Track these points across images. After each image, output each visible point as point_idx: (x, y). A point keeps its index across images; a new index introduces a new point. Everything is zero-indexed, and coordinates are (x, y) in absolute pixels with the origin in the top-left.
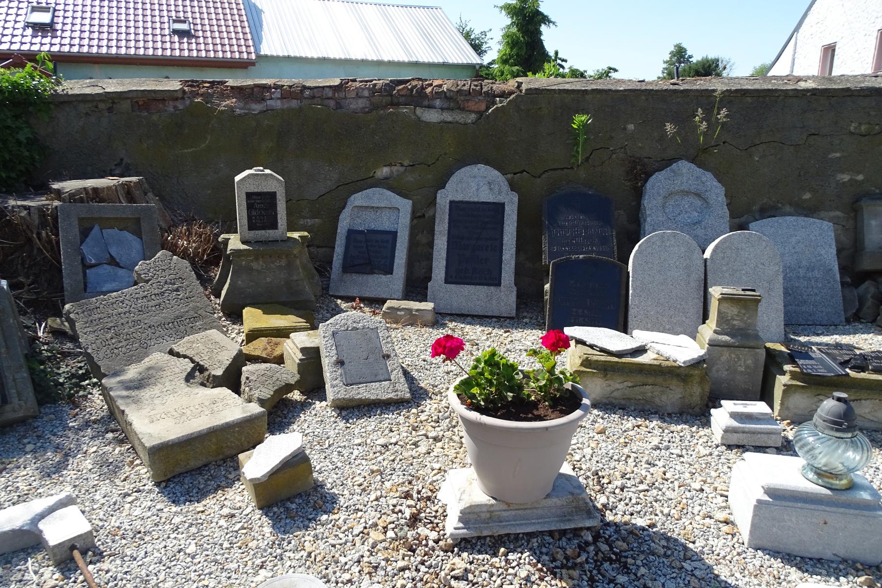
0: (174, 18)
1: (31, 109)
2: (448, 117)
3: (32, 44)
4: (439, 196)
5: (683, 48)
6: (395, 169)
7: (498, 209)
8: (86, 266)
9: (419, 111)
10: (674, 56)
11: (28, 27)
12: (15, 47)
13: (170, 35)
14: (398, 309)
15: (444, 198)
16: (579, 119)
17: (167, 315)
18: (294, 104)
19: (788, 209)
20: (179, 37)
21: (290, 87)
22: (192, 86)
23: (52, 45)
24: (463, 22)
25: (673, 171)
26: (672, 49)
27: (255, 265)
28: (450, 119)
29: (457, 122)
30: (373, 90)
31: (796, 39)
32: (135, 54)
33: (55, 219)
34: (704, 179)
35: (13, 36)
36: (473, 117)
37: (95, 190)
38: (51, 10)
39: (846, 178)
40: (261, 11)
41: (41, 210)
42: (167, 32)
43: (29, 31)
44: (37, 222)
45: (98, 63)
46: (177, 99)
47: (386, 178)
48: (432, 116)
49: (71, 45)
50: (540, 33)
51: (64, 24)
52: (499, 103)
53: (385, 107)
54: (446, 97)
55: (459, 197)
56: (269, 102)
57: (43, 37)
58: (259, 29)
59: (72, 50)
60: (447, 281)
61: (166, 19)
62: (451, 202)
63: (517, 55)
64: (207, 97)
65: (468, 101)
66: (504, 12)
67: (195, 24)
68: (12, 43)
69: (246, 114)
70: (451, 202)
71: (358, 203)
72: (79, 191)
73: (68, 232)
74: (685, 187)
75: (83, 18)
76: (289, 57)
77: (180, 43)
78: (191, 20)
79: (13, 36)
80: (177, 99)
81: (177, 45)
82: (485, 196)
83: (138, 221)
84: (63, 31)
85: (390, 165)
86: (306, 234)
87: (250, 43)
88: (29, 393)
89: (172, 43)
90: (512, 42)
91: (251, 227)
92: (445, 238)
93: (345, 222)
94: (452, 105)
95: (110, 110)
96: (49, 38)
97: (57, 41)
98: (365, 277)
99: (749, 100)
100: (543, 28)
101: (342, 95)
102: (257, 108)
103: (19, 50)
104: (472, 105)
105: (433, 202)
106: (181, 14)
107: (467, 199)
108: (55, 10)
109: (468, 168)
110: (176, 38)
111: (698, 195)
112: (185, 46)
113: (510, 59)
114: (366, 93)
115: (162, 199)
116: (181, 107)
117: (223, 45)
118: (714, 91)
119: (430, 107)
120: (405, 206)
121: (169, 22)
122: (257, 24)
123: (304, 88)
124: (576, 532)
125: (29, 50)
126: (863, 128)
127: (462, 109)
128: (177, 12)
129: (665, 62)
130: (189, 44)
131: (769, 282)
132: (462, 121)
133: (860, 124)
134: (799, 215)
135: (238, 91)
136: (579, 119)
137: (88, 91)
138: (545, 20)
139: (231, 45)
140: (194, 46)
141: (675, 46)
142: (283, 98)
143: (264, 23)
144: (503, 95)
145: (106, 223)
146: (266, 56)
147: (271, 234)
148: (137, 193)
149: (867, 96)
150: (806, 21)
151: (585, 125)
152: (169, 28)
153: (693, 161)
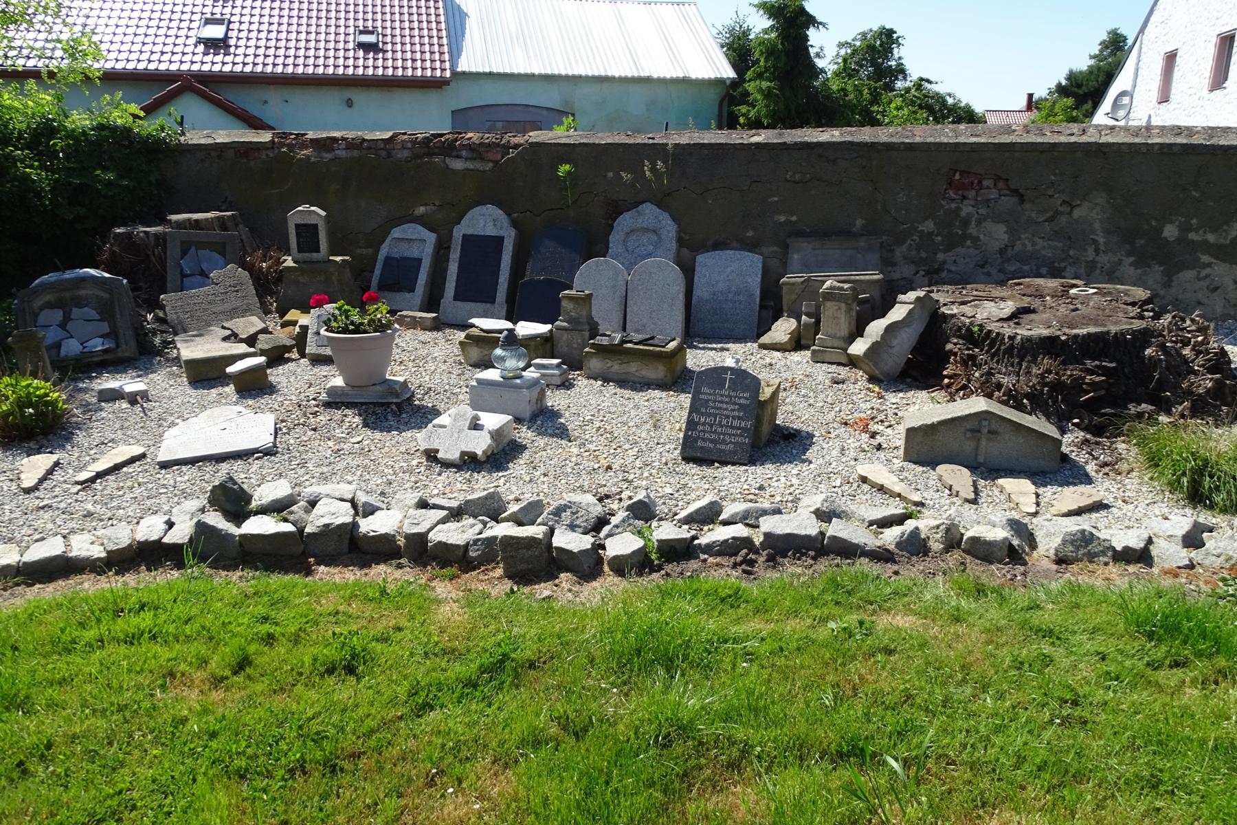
0: (361, 28)
1: (160, 156)
2: (470, 165)
3: (203, 63)
4: (455, 230)
5: (1121, 36)
6: (428, 207)
7: (500, 240)
8: (183, 276)
9: (448, 160)
10: (1107, 47)
11: (200, 43)
12: (185, 67)
13: (354, 49)
14: (406, 316)
15: (459, 232)
16: (565, 168)
17: (228, 306)
18: (355, 153)
19: (735, 244)
20: (364, 51)
21: (353, 139)
22: (281, 138)
23: (224, 63)
24: (741, 17)
25: (638, 212)
26: (1105, 37)
27: (301, 279)
28: (472, 167)
29: (478, 170)
30: (414, 142)
31: (1141, 43)
32: (313, 74)
33: (165, 241)
34: (661, 218)
35: (184, 54)
36: (490, 165)
37: (197, 221)
38: (226, 22)
39: (782, 218)
40: (466, 14)
41: (156, 235)
42: (351, 45)
43: (201, 48)
44: (153, 243)
45: (273, 84)
46: (268, 149)
47: (422, 216)
48: (457, 165)
49: (245, 64)
50: (806, 38)
51: (238, 39)
52: (512, 153)
53: (421, 157)
54: (471, 148)
55: (470, 232)
56: (337, 152)
57: (215, 54)
58: (460, 39)
59: (245, 70)
60: (456, 299)
61: (351, 30)
62: (464, 236)
63: (776, 68)
64: (291, 146)
65: (487, 152)
66: (761, 12)
67: (384, 36)
68: (182, 62)
69: (318, 162)
70: (464, 236)
71: (396, 235)
72: (185, 221)
73: (173, 250)
74: (645, 225)
75: (271, 16)
76: (491, 74)
77: (365, 59)
78: (380, 30)
79: (184, 54)
80: (268, 149)
81: (361, 62)
82: (490, 231)
83: (224, 245)
84: (237, 47)
85: (425, 205)
86: (347, 258)
87: (447, 57)
88: (133, 344)
89: (356, 59)
90: (767, 51)
91: (300, 251)
92: (457, 265)
93: (384, 251)
94: (475, 155)
95: (219, 157)
96: (222, 55)
97: (229, 59)
98: (395, 294)
99: (706, 152)
100: (811, 32)
101: (391, 146)
102: (327, 156)
103: (189, 70)
104: (491, 156)
105: (450, 236)
106: (370, 24)
107: (476, 233)
108: (230, 22)
109: (479, 208)
110: (361, 53)
111: (655, 231)
112: (371, 62)
113: (765, 72)
114: (409, 145)
115: (252, 230)
116: (271, 155)
117: (414, 60)
118: (667, 144)
119: (458, 157)
120: (431, 238)
121: (355, 34)
122: (459, 33)
123: (364, 140)
124: (389, 404)
125: (200, 71)
126: (797, 176)
127: (482, 159)
128: (365, 20)
129: (1092, 57)
130: (375, 59)
131: (672, 299)
132: (481, 169)
133: (794, 173)
134: (744, 250)
135: (315, 142)
136: (565, 168)
137: (203, 141)
138: (811, 21)
139: (423, 61)
140: (380, 63)
141: (1109, 33)
142: (347, 148)
143: (467, 31)
144: (516, 146)
145: (201, 245)
146: (464, 73)
147: (315, 256)
148: (229, 224)
149: (799, 149)
150: (1153, 19)
151: (569, 173)
152: (354, 41)
153: (659, 206)
